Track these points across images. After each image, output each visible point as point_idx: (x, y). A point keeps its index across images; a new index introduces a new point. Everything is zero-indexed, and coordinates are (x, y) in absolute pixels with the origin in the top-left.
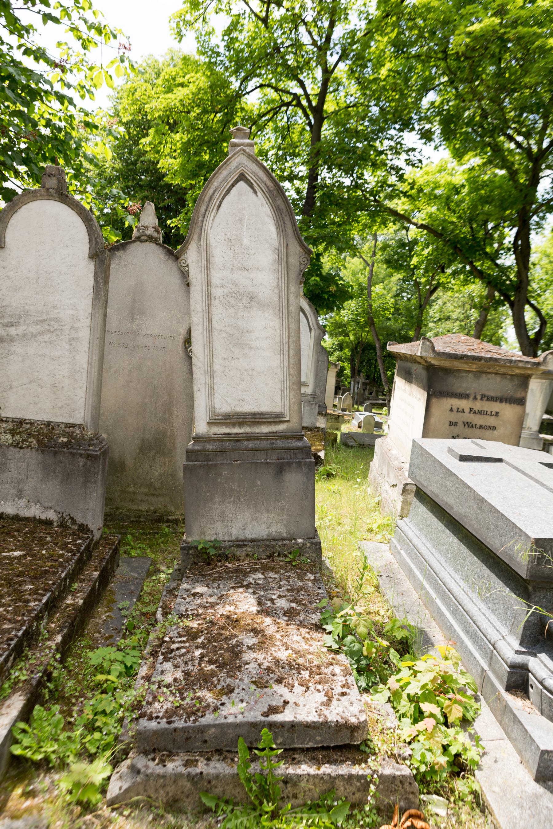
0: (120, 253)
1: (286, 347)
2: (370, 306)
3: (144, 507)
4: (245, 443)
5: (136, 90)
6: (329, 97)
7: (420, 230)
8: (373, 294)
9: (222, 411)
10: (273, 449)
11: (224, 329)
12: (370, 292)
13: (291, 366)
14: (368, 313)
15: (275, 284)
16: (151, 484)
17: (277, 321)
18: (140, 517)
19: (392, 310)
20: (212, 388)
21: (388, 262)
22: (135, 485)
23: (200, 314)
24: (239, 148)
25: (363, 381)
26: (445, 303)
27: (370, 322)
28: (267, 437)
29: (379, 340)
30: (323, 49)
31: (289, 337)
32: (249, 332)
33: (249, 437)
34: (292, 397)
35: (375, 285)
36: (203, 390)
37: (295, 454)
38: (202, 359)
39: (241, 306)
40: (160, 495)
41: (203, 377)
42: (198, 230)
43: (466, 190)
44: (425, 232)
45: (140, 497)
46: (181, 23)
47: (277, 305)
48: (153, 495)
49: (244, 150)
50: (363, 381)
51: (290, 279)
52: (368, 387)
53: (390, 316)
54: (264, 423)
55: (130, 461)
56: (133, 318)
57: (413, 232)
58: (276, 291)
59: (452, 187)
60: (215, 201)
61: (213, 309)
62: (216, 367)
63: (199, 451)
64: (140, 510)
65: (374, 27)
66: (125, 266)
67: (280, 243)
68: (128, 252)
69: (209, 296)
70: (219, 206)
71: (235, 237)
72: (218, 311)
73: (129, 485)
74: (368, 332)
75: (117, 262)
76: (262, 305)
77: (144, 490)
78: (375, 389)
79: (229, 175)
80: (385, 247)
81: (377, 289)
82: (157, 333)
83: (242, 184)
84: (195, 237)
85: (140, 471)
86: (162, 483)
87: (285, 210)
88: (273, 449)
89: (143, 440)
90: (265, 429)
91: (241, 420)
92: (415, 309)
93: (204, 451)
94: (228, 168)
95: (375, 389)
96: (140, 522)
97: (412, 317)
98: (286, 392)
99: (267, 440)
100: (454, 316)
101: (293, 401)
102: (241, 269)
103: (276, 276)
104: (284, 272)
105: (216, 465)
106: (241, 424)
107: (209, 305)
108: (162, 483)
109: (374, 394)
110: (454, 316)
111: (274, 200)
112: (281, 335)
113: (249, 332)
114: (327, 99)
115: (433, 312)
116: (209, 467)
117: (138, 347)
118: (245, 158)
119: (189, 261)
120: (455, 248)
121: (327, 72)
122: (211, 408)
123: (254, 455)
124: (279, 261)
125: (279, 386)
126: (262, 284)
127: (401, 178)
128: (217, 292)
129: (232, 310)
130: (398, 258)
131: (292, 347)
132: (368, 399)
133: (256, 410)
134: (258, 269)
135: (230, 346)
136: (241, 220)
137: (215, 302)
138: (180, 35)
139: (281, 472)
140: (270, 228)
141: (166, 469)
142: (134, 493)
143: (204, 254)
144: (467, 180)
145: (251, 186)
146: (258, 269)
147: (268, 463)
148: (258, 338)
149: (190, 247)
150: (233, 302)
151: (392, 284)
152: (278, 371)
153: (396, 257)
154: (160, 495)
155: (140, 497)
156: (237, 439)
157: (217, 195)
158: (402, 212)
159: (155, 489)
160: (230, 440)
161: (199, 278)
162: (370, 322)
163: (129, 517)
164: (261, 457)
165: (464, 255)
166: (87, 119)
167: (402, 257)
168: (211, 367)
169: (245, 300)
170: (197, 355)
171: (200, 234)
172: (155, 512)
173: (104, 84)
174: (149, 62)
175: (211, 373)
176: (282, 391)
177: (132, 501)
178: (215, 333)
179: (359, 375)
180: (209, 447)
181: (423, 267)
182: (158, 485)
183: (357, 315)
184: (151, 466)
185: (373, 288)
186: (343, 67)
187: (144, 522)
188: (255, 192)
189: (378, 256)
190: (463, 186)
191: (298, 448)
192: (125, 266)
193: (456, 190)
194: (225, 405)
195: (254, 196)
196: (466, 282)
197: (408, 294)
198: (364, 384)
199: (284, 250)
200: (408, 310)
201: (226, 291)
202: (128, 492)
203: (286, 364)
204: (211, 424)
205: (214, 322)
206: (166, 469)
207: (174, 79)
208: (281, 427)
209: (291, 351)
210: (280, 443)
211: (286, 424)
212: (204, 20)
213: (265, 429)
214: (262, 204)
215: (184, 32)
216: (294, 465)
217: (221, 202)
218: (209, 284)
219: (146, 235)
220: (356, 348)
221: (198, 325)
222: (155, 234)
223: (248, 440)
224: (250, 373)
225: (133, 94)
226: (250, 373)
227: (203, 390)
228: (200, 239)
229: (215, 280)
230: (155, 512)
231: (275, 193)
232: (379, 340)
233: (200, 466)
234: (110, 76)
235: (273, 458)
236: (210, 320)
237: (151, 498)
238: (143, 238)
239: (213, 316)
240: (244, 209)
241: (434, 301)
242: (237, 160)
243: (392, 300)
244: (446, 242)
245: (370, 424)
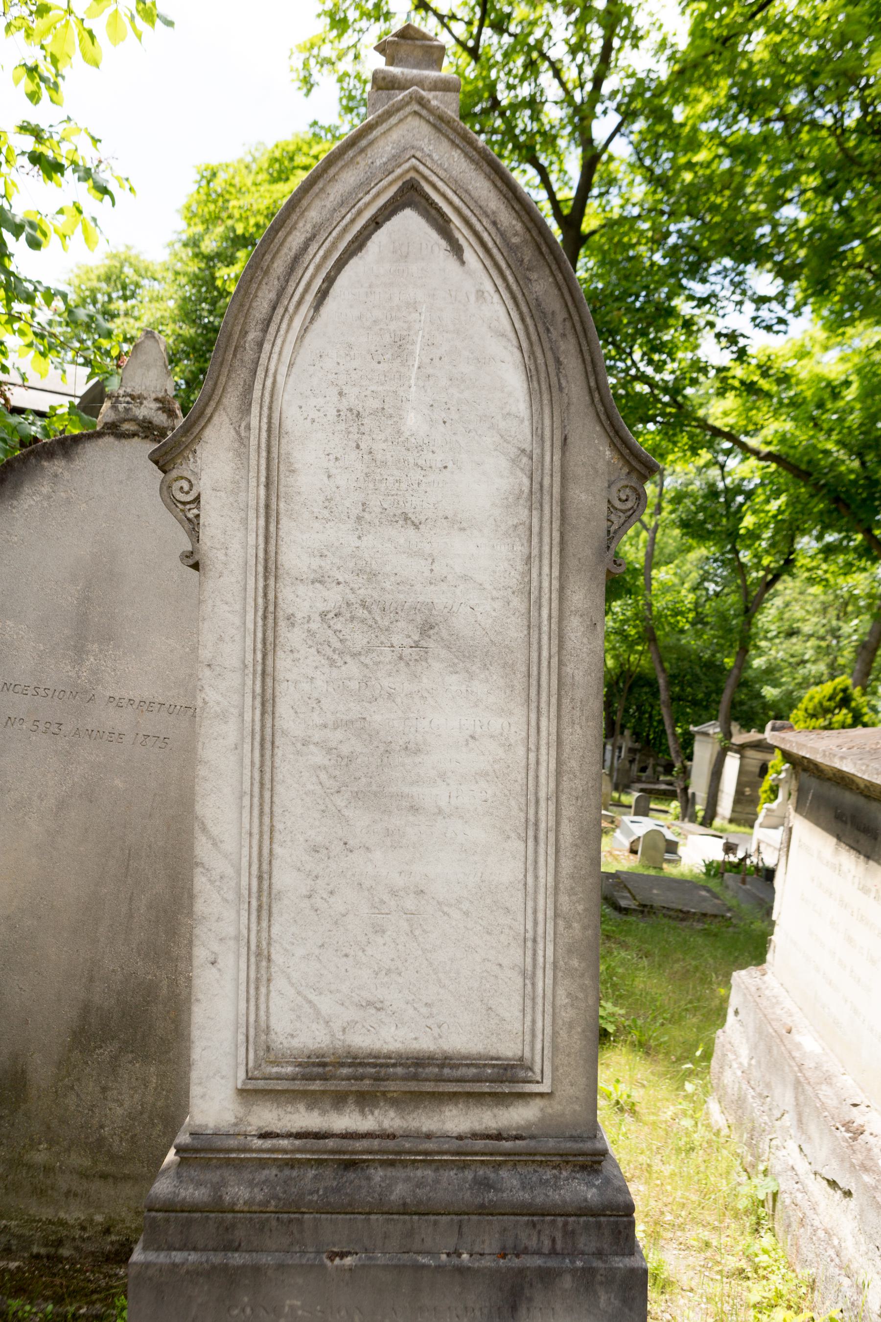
0: (57, 466)
1: (546, 817)
2: (650, 605)
3: (74, 1214)
4: (378, 1175)
5: (214, 175)
6: (592, 205)
7: (763, 464)
8: (655, 585)
9: (296, 1043)
10: (484, 1210)
11: (317, 736)
12: (649, 580)
13: (566, 883)
14: (645, 619)
15: (514, 580)
16: (101, 1140)
17: (519, 714)
18: (60, 1243)
19: (691, 616)
20: (261, 956)
21: (684, 524)
22: (51, 1142)
23: (233, 679)
24: (401, 96)
25: (630, 744)
26: (787, 605)
27: (649, 636)
28: (462, 1152)
29: (664, 670)
30: (581, 117)
31: (559, 773)
32: (412, 750)
33: (396, 1152)
34: (563, 999)
35: (658, 565)
36: (227, 961)
37: (569, 1234)
38: (229, 846)
39: (388, 655)
40: (126, 1178)
41: (229, 914)
42: (243, 374)
43: (851, 394)
44: (773, 466)
45: (63, 1182)
46: (312, 62)
47: (520, 657)
48: (104, 1176)
49: (422, 102)
50: (630, 744)
51: (572, 563)
52: (637, 757)
53: (687, 626)
54: (453, 1097)
55: (41, 1072)
56: (80, 651)
57: (742, 470)
58: (518, 603)
59: (823, 384)
60: (311, 275)
61: (283, 662)
62: (284, 878)
63: (194, 1208)
64: (62, 1223)
65: (689, 72)
66: (68, 501)
67: (538, 433)
68: (77, 464)
69: (270, 614)
70: (323, 294)
71: (376, 404)
72: (300, 670)
73: (33, 1145)
74: (641, 653)
75: (45, 490)
76: (465, 655)
77: (78, 1160)
78: (651, 761)
79: (364, 186)
80: (678, 499)
81: (662, 575)
82: (146, 695)
83: (409, 220)
84: (231, 400)
85: (71, 1101)
86: (133, 1140)
87: (561, 315)
88: (484, 1210)
89: (86, 1009)
90: (456, 1121)
91: (366, 1085)
92: (736, 616)
93: (217, 1206)
94: (363, 162)
95: (651, 761)
96: (60, 1259)
97: (730, 631)
98: (543, 982)
99: (464, 1166)
100: (807, 628)
101: (567, 1015)
102: (393, 521)
103: (520, 549)
104: (551, 535)
105: (257, 1269)
106: (365, 1100)
107: (268, 647)
108: (133, 1140)
109: (649, 771)
110: (807, 628)
111: (523, 281)
112: (532, 769)
113: (412, 750)
114: (588, 210)
115: (767, 618)
116: (230, 1277)
117: (90, 733)
118: (425, 129)
119: (204, 486)
120: (837, 500)
121: (591, 162)
122: (256, 1035)
123: (410, 1234)
124: (534, 497)
125: (515, 955)
126: (465, 578)
127: (741, 355)
128: (298, 599)
129: (353, 668)
130: (713, 518)
131: (568, 811)
132: (639, 780)
133: (426, 1044)
134: (456, 523)
135: (340, 801)
136: (400, 346)
137: (291, 636)
138: (308, 84)
139: (514, 1308)
140: (507, 376)
141: (150, 1099)
142: (48, 1170)
143: (257, 461)
144: (859, 371)
145: (442, 226)
146: (456, 523)
147: (461, 1271)
148: (443, 776)
149: (209, 433)
150: (358, 639)
151: (687, 567)
152: (516, 901)
153: (701, 516)
154: (126, 1178)
155: (63, 1182)
156: (346, 1159)
157: (316, 254)
158: (727, 429)
159: (113, 1157)
160: (320, 1162)
161: (235, 547)
162: (649, 636)
163: (26, 1242)
164: (437, 1244)
165: (855, 514)
166: (41, 149)
167: (712, 516)
168: (264, 876)
169: (402, 634)
170: (215, 831)
171: (249, 389)
172: (107, 1231)
173: (77, 56)
174: (257, 155)
175: (262, 900)
176: (528, 976)
177: (39, 1192)
178: (284, 749)
179: (622, 733)
180: (239, 1192)
181: (767, 534)
182: (120, 1147)
183: (624, 622)
184: (104, 1089)
185: (654, 573)
186: (621, 149)
187: (72, 1261)
188: (457, 250)
189: (664, 514)
190: (847, 383)
191: (584, 1211)
192: (68, 501)
193: (834, 391)
194: (305, 1026)
195: (452, 262)
196: (848, 569)
197: (716, 583)
198: (631, 750)
199: (551, 458)
200: (723, 617)
201: (333, 597)
202: (30, 1166)
203: (546, 876)
204: (250, 1093)
205: (283, 709)
206: (150, 1099)
207: (292, 159)
208: (518, 1116)
209: (566, 829)
210: (512, 1185)
211: (539, 1103)
212: (356, 57)
213: (456, 1121)
214: (480, 294)
215: (316, 77)
216: (567, 1282)
217: (330, 280)
218: (270, 568)
219: (134, 420)
220: (617, 683)
221: (223, 716)
222: (161, 419)
223: (392, 1163)
224: (410, 903)
225: (209, 182)
226: (410, 903)
227: (227, 961)
228: (245, 409)
229: (294, 556)
230: (107, 1231)
231: (528, 254)
232: (664, 670)
233: (195, 1274)
234: (90, 33)
235: (482, 1248)
236: (267, 703)
237: (96, 1185)
238: (126, 426)
239: (281, 688)
240: (413, 306)
241: (768, 600)
242: (395, 135)
243: (691, 597)
244: (817, 488)
245: (655, 847)
